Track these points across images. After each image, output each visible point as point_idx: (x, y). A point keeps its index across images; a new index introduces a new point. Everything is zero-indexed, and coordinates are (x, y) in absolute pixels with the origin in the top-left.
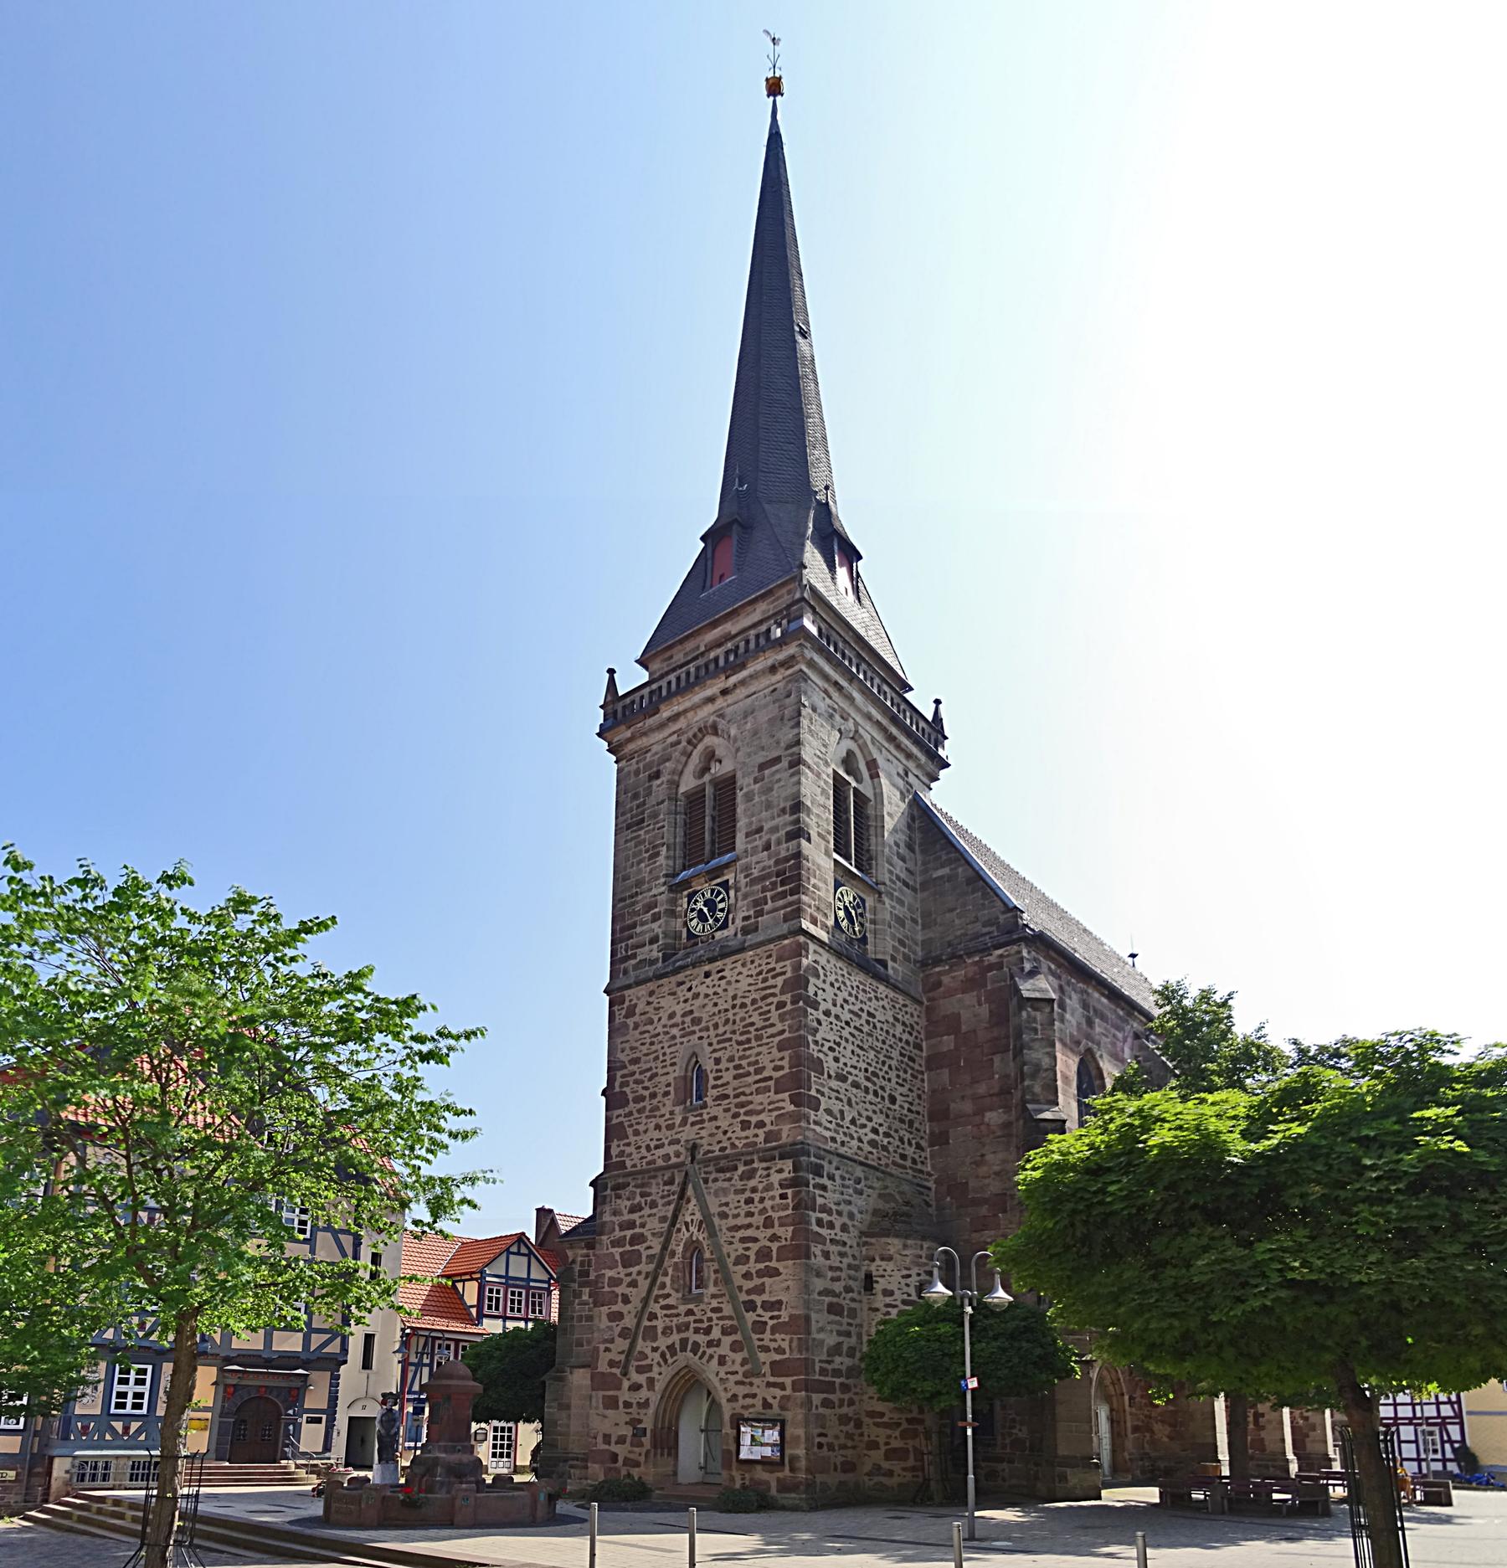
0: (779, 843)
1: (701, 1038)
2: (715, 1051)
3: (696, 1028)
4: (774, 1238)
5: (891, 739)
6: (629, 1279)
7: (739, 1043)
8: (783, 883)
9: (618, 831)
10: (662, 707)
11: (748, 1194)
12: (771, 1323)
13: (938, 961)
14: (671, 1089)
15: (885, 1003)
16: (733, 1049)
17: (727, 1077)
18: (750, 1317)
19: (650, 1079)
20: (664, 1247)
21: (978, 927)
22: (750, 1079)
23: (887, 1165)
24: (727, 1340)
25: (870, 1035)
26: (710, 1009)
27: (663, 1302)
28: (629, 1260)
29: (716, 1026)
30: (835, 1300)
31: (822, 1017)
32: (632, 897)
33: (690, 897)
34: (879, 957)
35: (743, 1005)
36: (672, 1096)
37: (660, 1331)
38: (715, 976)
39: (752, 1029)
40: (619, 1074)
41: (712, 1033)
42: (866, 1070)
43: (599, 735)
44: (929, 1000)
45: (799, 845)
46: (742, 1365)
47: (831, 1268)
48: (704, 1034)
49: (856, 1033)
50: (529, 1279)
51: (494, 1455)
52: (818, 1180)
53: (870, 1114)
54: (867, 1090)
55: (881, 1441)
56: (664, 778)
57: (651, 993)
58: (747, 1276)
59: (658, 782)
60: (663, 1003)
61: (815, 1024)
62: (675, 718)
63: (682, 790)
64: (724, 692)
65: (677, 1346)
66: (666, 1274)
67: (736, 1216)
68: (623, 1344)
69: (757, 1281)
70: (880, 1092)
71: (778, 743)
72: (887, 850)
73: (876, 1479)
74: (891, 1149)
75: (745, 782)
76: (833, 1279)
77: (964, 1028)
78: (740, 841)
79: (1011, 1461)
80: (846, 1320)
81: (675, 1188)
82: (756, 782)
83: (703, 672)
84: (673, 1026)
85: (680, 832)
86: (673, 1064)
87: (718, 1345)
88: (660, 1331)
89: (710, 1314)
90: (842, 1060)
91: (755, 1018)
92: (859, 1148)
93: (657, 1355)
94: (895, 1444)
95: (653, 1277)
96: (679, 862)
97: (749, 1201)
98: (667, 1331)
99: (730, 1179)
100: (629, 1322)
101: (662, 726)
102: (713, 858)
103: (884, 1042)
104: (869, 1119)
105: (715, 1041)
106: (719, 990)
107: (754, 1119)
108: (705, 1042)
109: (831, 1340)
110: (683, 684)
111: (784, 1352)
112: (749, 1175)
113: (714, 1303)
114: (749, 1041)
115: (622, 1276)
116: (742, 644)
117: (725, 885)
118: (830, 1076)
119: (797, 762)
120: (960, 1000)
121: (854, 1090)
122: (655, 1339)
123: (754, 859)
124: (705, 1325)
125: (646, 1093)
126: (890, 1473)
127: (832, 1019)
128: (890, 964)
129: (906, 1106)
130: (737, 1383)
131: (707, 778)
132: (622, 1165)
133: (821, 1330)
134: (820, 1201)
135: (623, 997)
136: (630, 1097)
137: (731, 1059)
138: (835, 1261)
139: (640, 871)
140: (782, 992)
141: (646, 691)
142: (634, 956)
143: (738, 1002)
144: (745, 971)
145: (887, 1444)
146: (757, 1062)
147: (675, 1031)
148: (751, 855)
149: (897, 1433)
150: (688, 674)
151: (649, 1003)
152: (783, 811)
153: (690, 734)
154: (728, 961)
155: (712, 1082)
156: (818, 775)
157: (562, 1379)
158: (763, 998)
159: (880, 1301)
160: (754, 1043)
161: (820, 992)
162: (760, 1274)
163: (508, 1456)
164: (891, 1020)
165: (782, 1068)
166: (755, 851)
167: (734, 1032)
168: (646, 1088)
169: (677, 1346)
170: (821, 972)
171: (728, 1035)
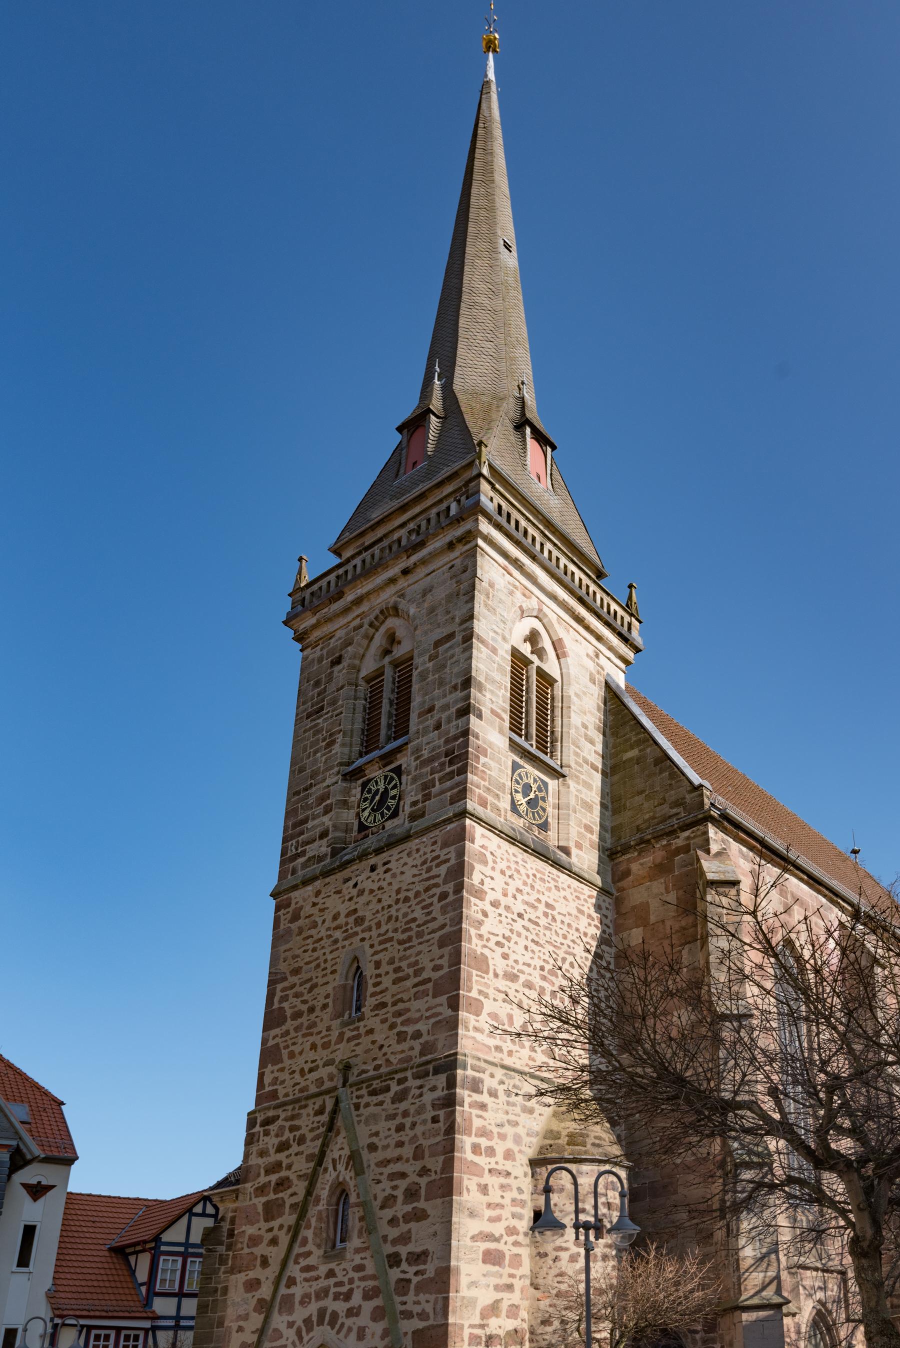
0: (449, 721)
1: (363, 940)
2: (376, 953)
3: (359, 929)
5: (579, 620)
6: (270, 1236)
7: (400, 943)
8: (451, 763)
9: (298, 721)
10: (346, 590)
11: (399, 1120)
12: (415, 1280)
13: (626, 849)
14: (330, 1001)
15: (567, 893)
16: (394, 950)
17: (387, 982)
18: (395, 1274)
19: (310, 990)
20: (309, 1193)
21: (665, 809)
22: (408, 983)
24: (368, 1307)
25: (546, 928)
26: (375, 906)
27: (303, 1263)
28: (271, 1211)
29: (379, 925)
30: (492, 1246)
32: (306, 789)
35: (407, 900)
36: (330, 1010)
37: (297, 1299)
38: (381, 869)
39: (413, 925)
40: (279, 987)
41: (374, 933)
42: (542, 968)
43: (286, 623)
44: (619, 890)
45: (469, 720)
46: (382, 1338)
47: (489, 1205)
48: (366, 935)
52: (476, 1097)
56: (345, 663)
57: (318, 894)
58: (393, 1222)
59: (340, 666)
60: (329, 903)
61: (480, 916)
62: (358, 601)
63: (363, 674)
64: (406, 572)
65: (315, 1319)
66: (308, 1227)
67: (386, 1147)
68: (257, 1320)
69: (404, 1227)
71: (453, 619)
72: (573, 731)
75: (422, 663)
76: (492, 1220)
77: (653, 919)
80: (508, 1270)
81: (325, 1118)
82: (430, 660)
84: (336, 928)
85: (359, 716)
86: (333, 972)
87: (357, 1315)
88: (297, 1299)
89: (352, 1274)
90: (513, 957)
91: (418, 913)
95: (295, 1232)
96: (356, 749)
97: (400, 1128)
98: (305, 1300)
99: (381, 1103)
100: (265, 1291)
101: (346, 610)
102: (387, 743)
103: (565, 937)
105: (376, 943)
106: (384, 884)
107: (410, 1029)
108: (367, 944)
109: (486, 1297)
110: (368, 565)
111: (427, 1318)
112: (400, 1097)
113: (357, 1260)
114: (410, 939)
115: (262, 1232)
117: (398, 771)
118: (496, 975)
120: (648, 888)
122: (291, 1311)
123: (425, 740)
124: (344, 1289)
125: (304, 1007)
127: (501, 910)
128: (574, 851)
131: (387, 659)
132: (274, 1095)
133: (474, 1284)
134: (477, 1123)
135: (290, 899)
136: (289, 1013)
137: (391, 962)
138: (495, 1195)
139: (316, 761)
140: (445, 882)
141: (332, 577)
143: (402, 896)
144: (410, 862)
146: (416, 963)
147: (338, 934)
150: (373, 556)
151: (314, 904)
152: (455, 688)
153: (372, 617)
154: (395, 851)
155: (371, 989)
156: (494, 651)
158: (427, 890)
160: (415, 941)
161: (487, 881)
162: (409, 1218)
164: (574, 912)
166: (426, 731)
167: (396, 930)
168: (304, 1002)
171: (390, 934)
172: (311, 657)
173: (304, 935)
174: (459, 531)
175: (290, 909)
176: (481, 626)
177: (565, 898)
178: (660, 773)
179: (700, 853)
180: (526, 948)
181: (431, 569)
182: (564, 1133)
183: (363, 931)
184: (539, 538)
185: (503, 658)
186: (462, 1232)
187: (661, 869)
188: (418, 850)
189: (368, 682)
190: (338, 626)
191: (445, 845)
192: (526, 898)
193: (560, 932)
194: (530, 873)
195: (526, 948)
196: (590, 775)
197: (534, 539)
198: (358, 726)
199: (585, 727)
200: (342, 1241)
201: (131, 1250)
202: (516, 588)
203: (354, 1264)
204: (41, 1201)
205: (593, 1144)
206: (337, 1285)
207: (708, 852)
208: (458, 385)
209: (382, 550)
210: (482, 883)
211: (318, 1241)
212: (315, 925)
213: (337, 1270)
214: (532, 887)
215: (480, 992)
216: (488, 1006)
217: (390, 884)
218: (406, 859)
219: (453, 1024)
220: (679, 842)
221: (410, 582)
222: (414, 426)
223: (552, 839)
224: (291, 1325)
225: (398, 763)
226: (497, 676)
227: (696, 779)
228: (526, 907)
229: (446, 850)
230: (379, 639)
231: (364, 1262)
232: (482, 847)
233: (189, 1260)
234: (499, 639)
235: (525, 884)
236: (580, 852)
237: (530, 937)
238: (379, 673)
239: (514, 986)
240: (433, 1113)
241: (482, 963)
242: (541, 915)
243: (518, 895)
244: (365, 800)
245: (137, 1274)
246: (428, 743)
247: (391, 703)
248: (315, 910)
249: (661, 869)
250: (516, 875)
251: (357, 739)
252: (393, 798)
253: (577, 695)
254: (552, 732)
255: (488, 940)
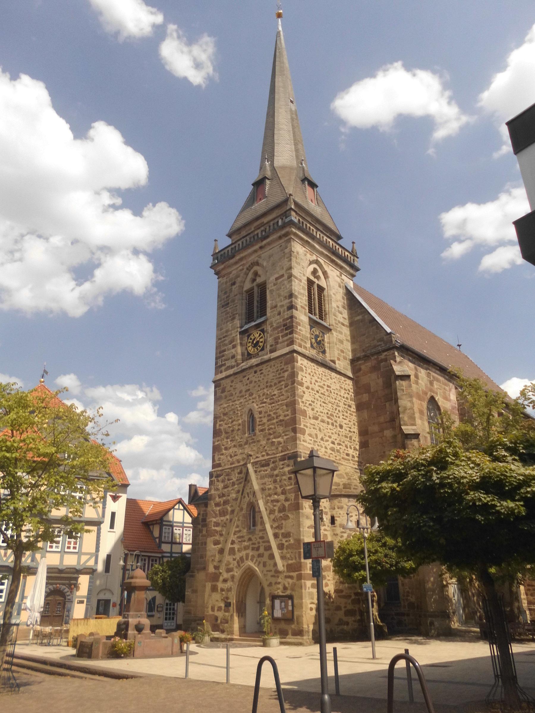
0: (284, 312)
4: (287, 500)
5: (333, 261)
8: (286, 329)
9: (218, 309)
12: (286, 544)
15: (335, 380)
17: (265, 420)
23: (340, 460)
25: (329, 396)
31: (305, 390)
32: (224, 337)
33: (248, 336)
34: (332, 359)
38: (259, 373)
42: (327, 413)
43: (211, 267)
45: (292, 312)
48: (254, 400)
49: (322, 396)
50: (183, 523)
51: (166, 619)
53: (330, 434)
54: (328, 423)
55: (343, 606)
56: (237, 285)
59: (235, 286)
62: (241, 259)
63: (245, 289)
64: (261, 248)
65: (245, 558)
70: (335, 424)
72: (333, 310)
73: (341, 627)
74: (341, 451)
75: (270, 287)
77: (372, 390)
78: (268, 310)
79: (408, 615)
83: (252, 239)
85: (244, 307)
89: (259, 540)
90: (316, 409)
92: (326, 452)
93: (235, 562)
94: (350, 607)
101: (236, 263)
103: (336, 399)
104: (330, 437)
106: (261, 379)
110: (244, 244)
112: (274, 469)
116: (268, 228)
118: (310, 418)
119: (290, 276)
121: (322, 424)
122: (234, 554)
124: (256, 546)
126: (347, 624)
128: (337, 362)
129: (348, 429)
130: (272, 576)
131: (255, 284)
141: (229, 248)
142: (224, 365)
144: (271, 370)
145: (345, 607)
148: (273, 318)
149: (350, 601)
150: (246, 240)
151: (231, 386)
153: (247, 266)
155: (258, 423)
156: (300, 281)
157: (192, 576)
159: (339, 530)
161: (304, 378)
163: (173, 619)
164: (339, 388)
165: (288, 415)
169: (245, 558)
170: (304, 368)
172: (222, 282)
173: (228, 398)
174: (283, 232)
175: (221, 388)
176: (295, 272)
177: (335, 382)
178: (372, 327)
179: (392, 362)
180: (321, 405)
181: (272, 247)
182: (341, 483)
183: (253, 399)
184: (315, 230)
185: (304, 283)
186: (304, 525)
187: (375, 369)
188: (274, 366)
189: (247, 292)
190: (233, 269)
191: (286, 364)
192: (319, 384)
193: (333, 397)
194: (320, 373)
195: (321, 405)
196: (341, 328)
197: (313, 230)
198: (244, 311)
199: (338, 307)
200: (254, 526)
201: (151, 523)
202: (307, 252)
203: (260, 536)
204: (117, 502)
205: (354, 489)
206: (253, 544)
207: (395, 361)
208: (276, 164)
209: (250, 238)
210: (302, 379)
211: (243, 526)
212: (232, 395)
213: (252, 538)
214: (321, 379)
215: (304, 425)
216: (308, 431)
217: (263, 379)
218: (269, 369)
219: (295, 439)
220: (383, 356)
221: (263, 252)
222: (259, 184)
223: (328, 357)
224: (234, 560)
225: (263, 328)
226: (302, 291)
227: (389, 330)
228: (320, 388)
229: (286, 366)
230: (250, 275)
231: (264, 535)
232: (301, 364)
233: (185, 529)
234: (302, 275)
235: (318, 378)
236: (340, 362)
237: (322, 400)
238: (252, 289)
239: (317, 422)
240: (289, 476)
241: (304, 413)
242: (326, 391)
243: (316, 383)
244: (249, 342)
245: (154, 533)
246: (276, 321)
247: (258, 302)
248: (232, 389)
249: (375, 369)
250: (315, 375)
251: (244, 317)
252: (262, 342)
253: (334, 294)
254: (325, 311)
255: (306, 403)
